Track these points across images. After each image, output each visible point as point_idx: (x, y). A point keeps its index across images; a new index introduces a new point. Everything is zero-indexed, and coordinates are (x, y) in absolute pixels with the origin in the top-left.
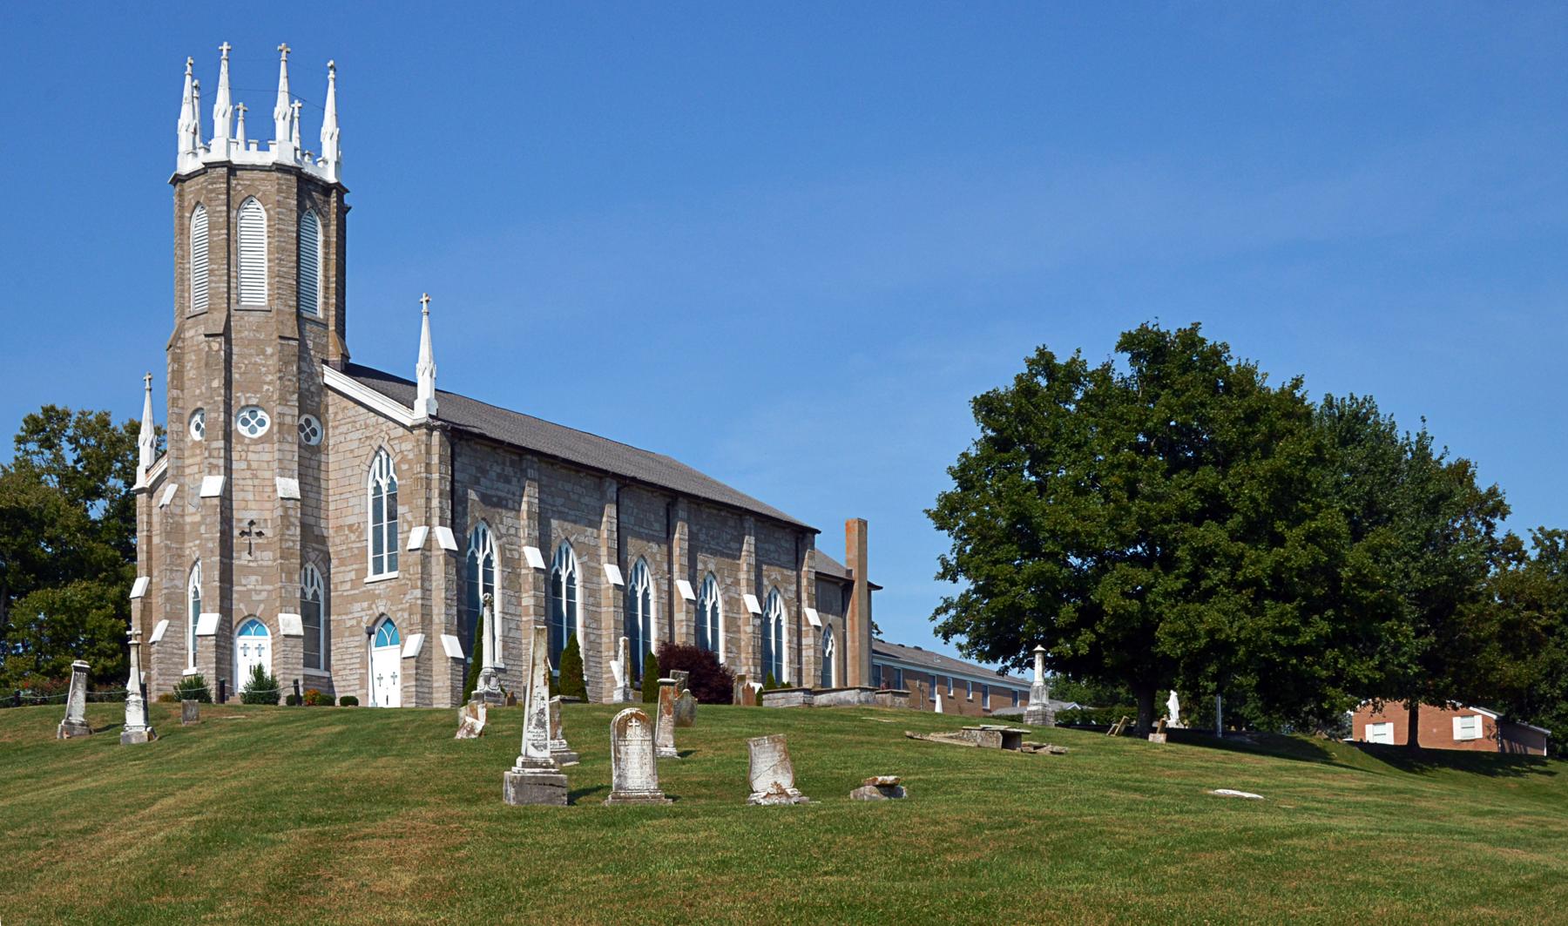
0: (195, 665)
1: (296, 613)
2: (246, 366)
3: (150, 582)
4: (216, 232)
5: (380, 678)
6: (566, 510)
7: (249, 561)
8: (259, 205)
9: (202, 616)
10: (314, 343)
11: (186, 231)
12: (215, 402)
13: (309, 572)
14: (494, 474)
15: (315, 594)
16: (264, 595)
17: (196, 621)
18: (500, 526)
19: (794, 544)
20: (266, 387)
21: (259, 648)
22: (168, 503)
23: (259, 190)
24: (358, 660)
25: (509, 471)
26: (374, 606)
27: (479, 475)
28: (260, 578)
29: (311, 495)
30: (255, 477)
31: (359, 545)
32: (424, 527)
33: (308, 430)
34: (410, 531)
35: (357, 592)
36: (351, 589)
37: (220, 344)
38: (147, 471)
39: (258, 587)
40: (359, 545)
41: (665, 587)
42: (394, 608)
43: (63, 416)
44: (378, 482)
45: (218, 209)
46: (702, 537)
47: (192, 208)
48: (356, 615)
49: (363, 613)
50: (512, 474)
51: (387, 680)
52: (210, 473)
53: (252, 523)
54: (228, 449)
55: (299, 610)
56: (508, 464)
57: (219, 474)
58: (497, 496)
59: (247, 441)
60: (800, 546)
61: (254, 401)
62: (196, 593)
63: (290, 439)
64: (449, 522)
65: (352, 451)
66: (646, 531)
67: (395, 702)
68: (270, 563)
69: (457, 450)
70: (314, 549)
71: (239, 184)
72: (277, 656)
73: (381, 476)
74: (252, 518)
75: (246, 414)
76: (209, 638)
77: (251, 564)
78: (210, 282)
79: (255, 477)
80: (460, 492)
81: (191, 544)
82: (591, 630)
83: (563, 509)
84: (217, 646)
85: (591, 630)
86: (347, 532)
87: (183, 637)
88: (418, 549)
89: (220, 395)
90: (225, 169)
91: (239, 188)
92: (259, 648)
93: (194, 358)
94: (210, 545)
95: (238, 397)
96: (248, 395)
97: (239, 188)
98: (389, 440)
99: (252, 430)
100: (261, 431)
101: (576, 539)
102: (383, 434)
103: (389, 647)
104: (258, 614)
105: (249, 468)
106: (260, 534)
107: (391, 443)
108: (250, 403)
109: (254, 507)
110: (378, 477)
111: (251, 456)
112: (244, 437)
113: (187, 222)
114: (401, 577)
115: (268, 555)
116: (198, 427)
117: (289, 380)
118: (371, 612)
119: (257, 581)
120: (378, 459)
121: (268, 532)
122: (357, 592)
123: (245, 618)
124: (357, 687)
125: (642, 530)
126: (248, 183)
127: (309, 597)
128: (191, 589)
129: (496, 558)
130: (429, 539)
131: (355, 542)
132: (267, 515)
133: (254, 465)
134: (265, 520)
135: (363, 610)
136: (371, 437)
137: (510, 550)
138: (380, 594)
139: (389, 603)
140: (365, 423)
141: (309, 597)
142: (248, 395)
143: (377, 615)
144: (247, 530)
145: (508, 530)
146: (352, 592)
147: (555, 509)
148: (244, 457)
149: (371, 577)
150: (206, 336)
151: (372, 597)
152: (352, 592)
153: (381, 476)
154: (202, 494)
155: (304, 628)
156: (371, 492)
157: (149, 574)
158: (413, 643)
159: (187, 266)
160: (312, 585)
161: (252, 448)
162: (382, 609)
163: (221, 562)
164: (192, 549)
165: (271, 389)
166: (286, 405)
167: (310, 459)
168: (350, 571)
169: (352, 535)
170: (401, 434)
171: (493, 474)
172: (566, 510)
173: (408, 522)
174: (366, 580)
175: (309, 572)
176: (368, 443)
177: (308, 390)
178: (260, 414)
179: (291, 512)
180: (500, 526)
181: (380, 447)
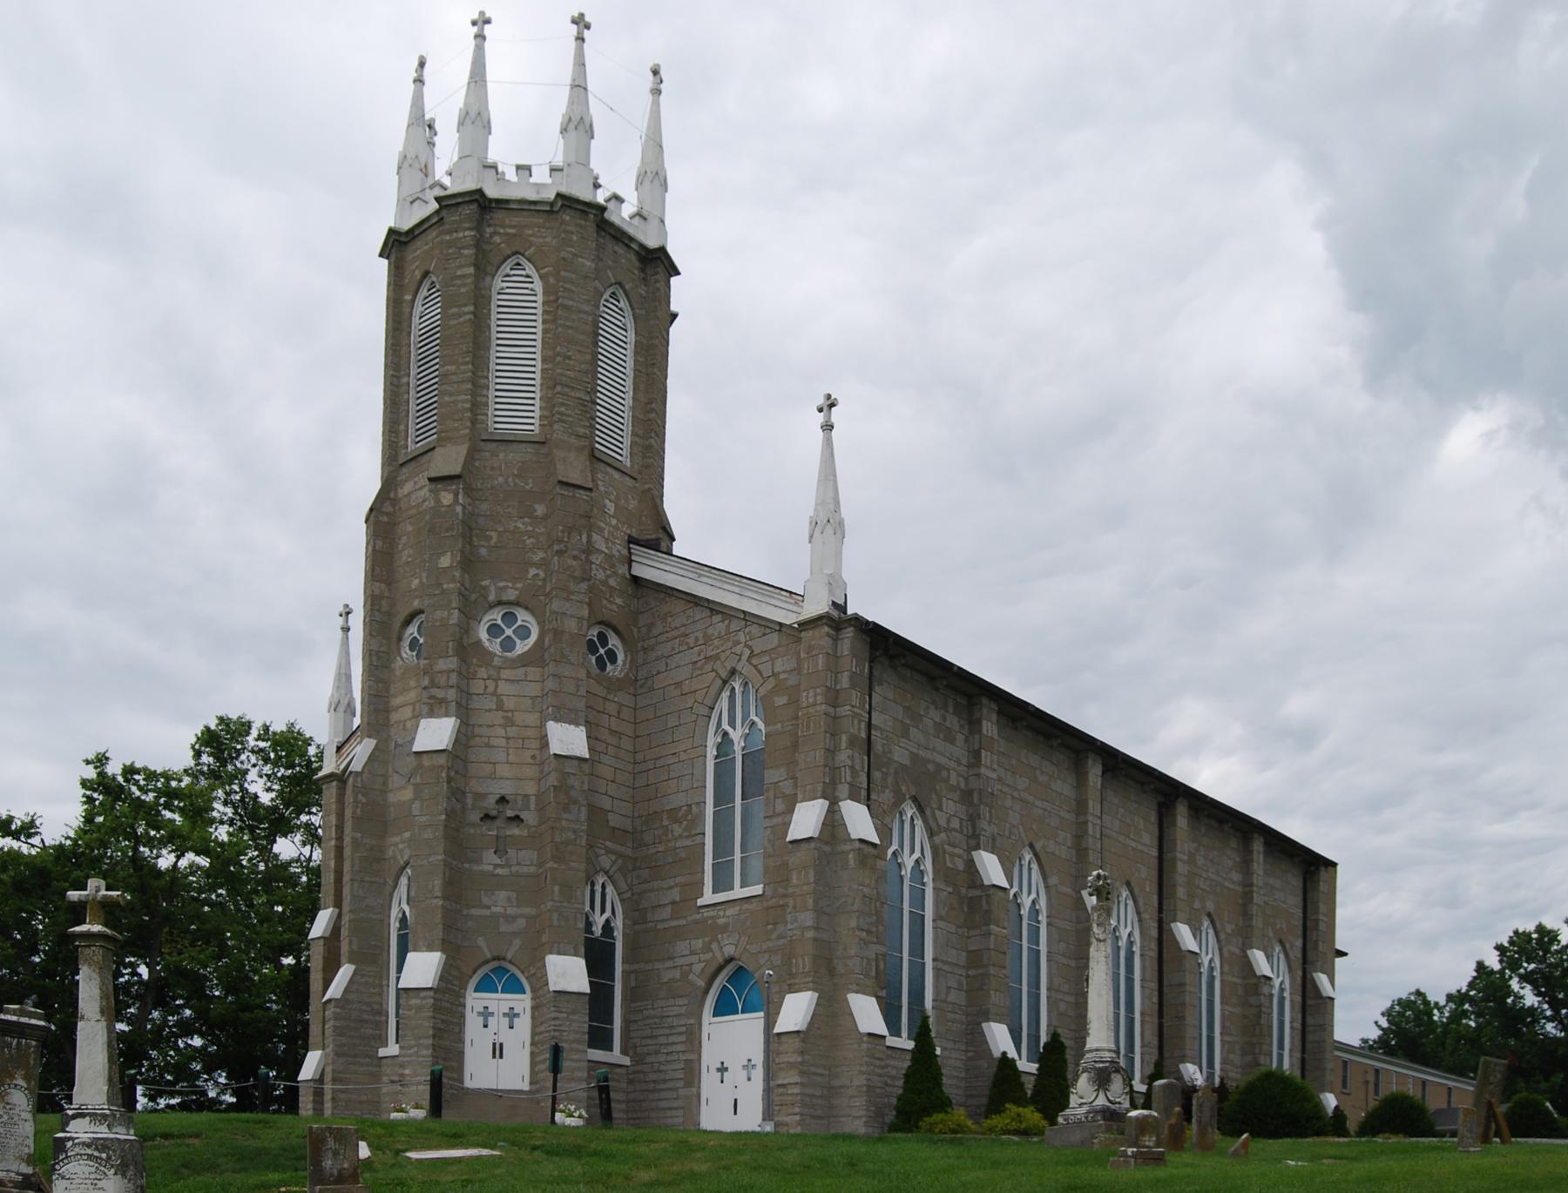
0: (397, 1042)
1: (576, 955)
2: (500, 534)
3: (340, 916)
4: (455, 310)
5: (722, 1069)
6: (1031, 798)
7: (496, 866)
8: (530, 269)
9: (410, 956)
10: (616, 505)
11: (405, 324)
12: (443, 591)
13: (598, 888)
14: (930, 723)
15: (608, 928)
16: (521, 922)
17: (400, 969)
18: (937, 812)
19: (1301, 880)
20: (533, 571)
21: (512, 1015)
22: (359, 769)
23: (531, 244)
24: (683, 1038)
25: (953, 722)
26: (714, 946)
27: (908, 721)
28: (514, 895)
29: (605, 759)
30: (510, 722)
31: (688, 842)
32: (821, 801)
33: (602, 651)
34: (791, 811)
35: (683, 922)
36: (672, 918)
37: (456, 495)
38: (339, 749)
39: (510, 911)
40: (688, 842)
41: (1154, 933)
42: (754, 948)
43: (245, 727)
44: (726, 734)
45: (459, 273)
46: (1200, 861)
47: (413, 288)
48: (680, 961)
49: (694, 958)
50: (957, 728)
51: (736, 1074)
52: (431, 714)
53: (503, 800)
54: (466, 675)
55: (583, 950)
56: (951, 710)
57: (447, 715)
58: (934, 762)
59: (497, 662)
60: (1308, 884)
61: (511, 595)
62: (403, 920)
63: (573, 659)
64: (864, 793)
65: (678, 684)
66: (1134, 844)
67: (751, 1119)
68: (532, 869)
69: (876, 673)
70: (608, 851)
71: (495, 233)
72: (542, 1028)
73: (732, 724)
74: (503, 792)
75: (496, 616)
76: (423, 994)
77: (499, 871)
78: (442, 394)
79: (510, 722)
80: (878, 747)
81: (398, 839)
82: (1060, 996)
83: (1024, 795)
84: (436, 1008)
85: (1060, 996)
86: (665, 823)
87: (380, 995)
88: (810, 839)
89: (453, 579)
90: (474, 206)
91: (497, 239)
92: (512, 1015)
93: (410, 528)
94: (428, 834)
95: (485, 588)
96: (501, 584)
97: (497, 239)
98: (752, 655)
99: (508, 645)
100: (522, 647)
101: (1043, 847)
102: (738, 649)
103: (740, 1016)
104: (509, 956)
105: (500, 706)
106: (517, 819)
107: (755, 662)
108: (505, 598)
109: (507, 775)
110: (726, 726)
111: (503, 688)
112: (493, 655)
113: (407, 310)
114: (769, 893)
115: (528, 856)
116: (414, 644)
117: (575, 558)
118: (709, 956)
119: (509, 899)
120: (725, 695)
121: (529, 817)
122: (683, 922)
123: (487, 962)
124: (681, 1084)
125: (1128, 842)
126: (512, 231)
127: (598, 930)
128: (395, 913)
129: (928, 865)
130: (833, 822)
131: (680, 836)
132: (530, 788)
133: (509, 703)
134: (526, 796)
135: (693, 953)
136: (716, 657)
137: (952, 855)
138: (726, 926)
139: (744, 939)
140: (705, 635)
141: (598, 930)
142: (501, 584)
143: (721, 960)
144: (494, 813)
145: (948, 821)
146: (674, 923)
147: (1015, 794)
148: (491, 689)
149: (708, 897)
150: (430, 480)
151: (712, 930)
152: (674, 923)
153: (732, 724)
154: (416, 748)
155: (590, 982)
156: (711, 752)
157: (338, 904)
158: (796, 1010)
159: (405, 380)
160: (603, 911)
161: (505, 674)
162: (729, 950)
163: (446, 863)
164: (398, 847)
165: (542, 575)
166: (568, 599)
167: (605, 699)
168: (671, 888)
169: (675, 826)
170: (775, 643)
171: (928, 723)
172: (1031, 798)
173: (784, 796)
174: (700, 902)
175: (598, 888)
176: (708, 667)
177: (605, 583)
178: (523, 617)
179: (571, 781)
180: (937, 812)
181: (733, 672)
